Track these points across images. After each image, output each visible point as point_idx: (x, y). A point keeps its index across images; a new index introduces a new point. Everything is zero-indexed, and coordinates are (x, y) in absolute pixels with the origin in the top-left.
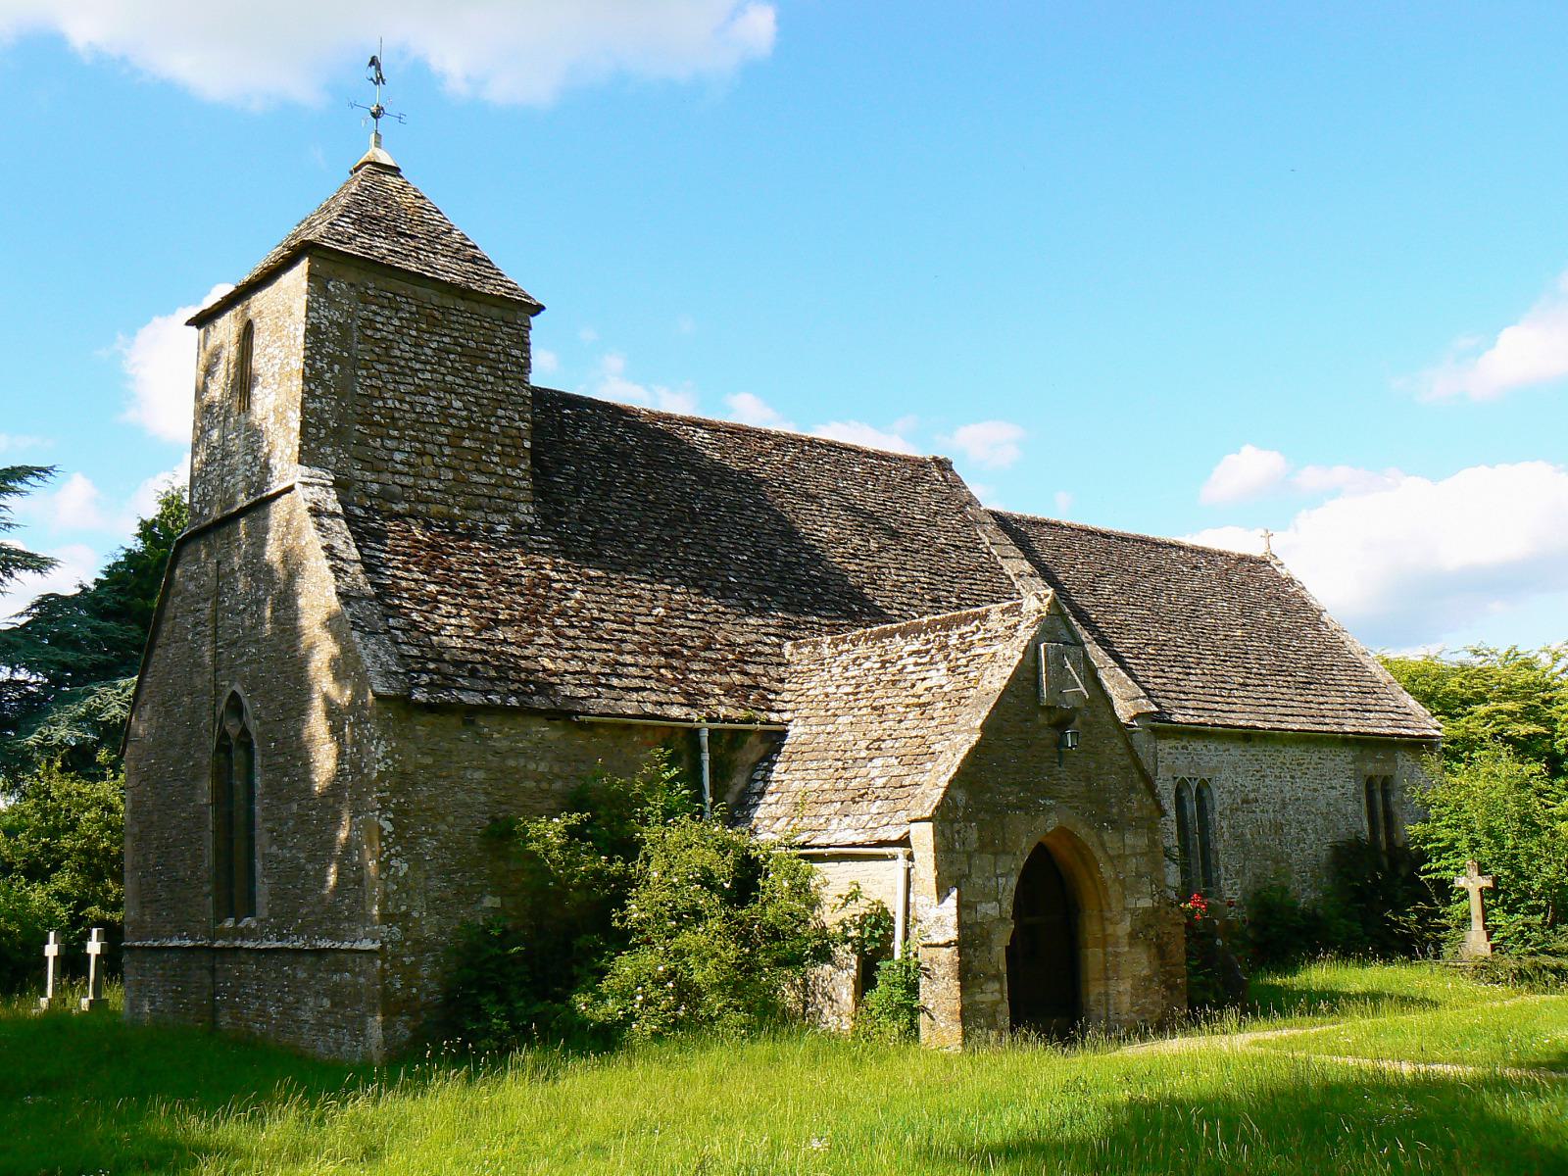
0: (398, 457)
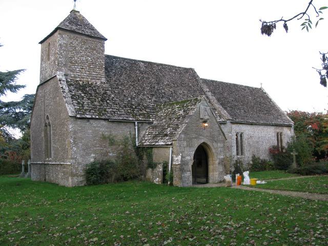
0: (77, 69)
